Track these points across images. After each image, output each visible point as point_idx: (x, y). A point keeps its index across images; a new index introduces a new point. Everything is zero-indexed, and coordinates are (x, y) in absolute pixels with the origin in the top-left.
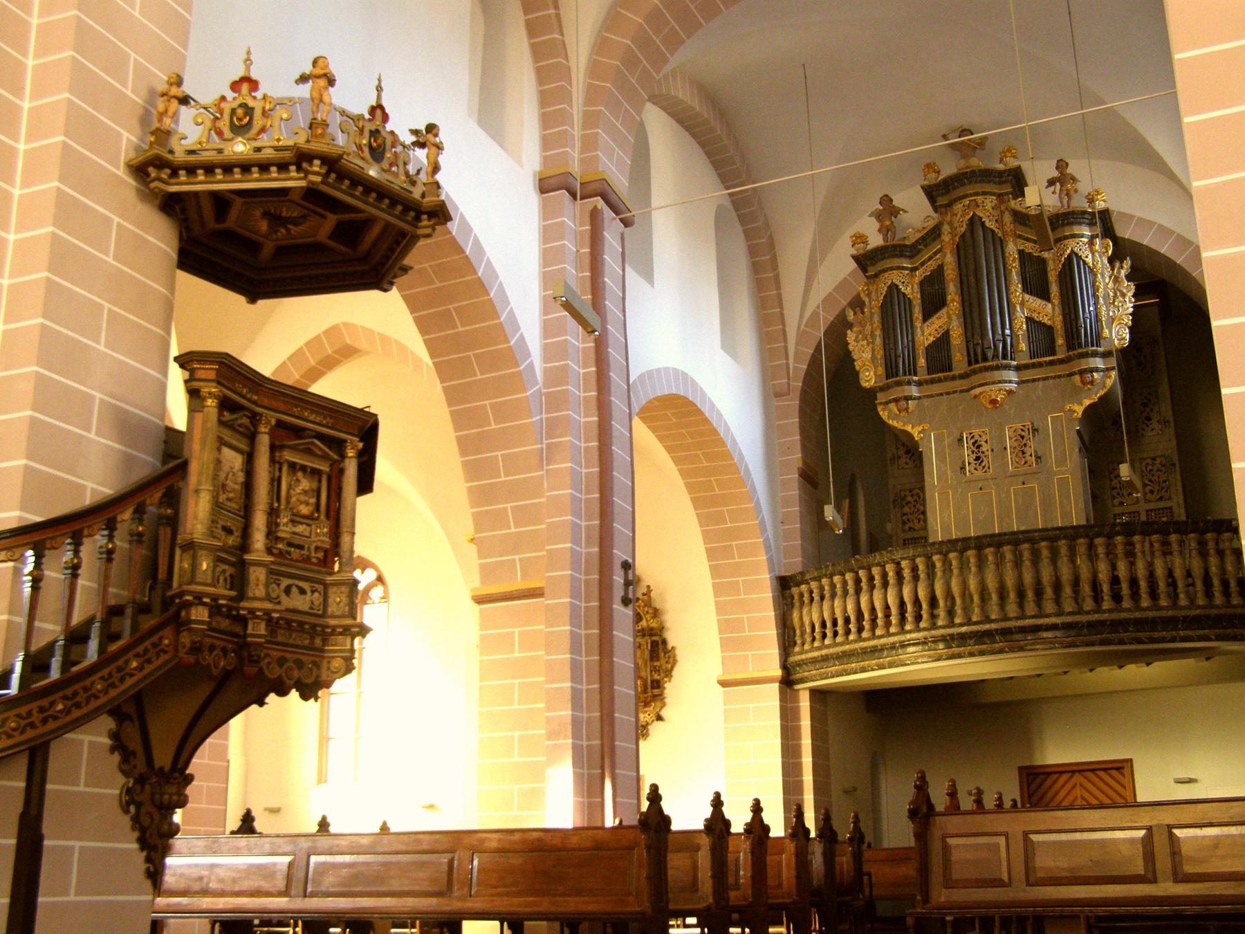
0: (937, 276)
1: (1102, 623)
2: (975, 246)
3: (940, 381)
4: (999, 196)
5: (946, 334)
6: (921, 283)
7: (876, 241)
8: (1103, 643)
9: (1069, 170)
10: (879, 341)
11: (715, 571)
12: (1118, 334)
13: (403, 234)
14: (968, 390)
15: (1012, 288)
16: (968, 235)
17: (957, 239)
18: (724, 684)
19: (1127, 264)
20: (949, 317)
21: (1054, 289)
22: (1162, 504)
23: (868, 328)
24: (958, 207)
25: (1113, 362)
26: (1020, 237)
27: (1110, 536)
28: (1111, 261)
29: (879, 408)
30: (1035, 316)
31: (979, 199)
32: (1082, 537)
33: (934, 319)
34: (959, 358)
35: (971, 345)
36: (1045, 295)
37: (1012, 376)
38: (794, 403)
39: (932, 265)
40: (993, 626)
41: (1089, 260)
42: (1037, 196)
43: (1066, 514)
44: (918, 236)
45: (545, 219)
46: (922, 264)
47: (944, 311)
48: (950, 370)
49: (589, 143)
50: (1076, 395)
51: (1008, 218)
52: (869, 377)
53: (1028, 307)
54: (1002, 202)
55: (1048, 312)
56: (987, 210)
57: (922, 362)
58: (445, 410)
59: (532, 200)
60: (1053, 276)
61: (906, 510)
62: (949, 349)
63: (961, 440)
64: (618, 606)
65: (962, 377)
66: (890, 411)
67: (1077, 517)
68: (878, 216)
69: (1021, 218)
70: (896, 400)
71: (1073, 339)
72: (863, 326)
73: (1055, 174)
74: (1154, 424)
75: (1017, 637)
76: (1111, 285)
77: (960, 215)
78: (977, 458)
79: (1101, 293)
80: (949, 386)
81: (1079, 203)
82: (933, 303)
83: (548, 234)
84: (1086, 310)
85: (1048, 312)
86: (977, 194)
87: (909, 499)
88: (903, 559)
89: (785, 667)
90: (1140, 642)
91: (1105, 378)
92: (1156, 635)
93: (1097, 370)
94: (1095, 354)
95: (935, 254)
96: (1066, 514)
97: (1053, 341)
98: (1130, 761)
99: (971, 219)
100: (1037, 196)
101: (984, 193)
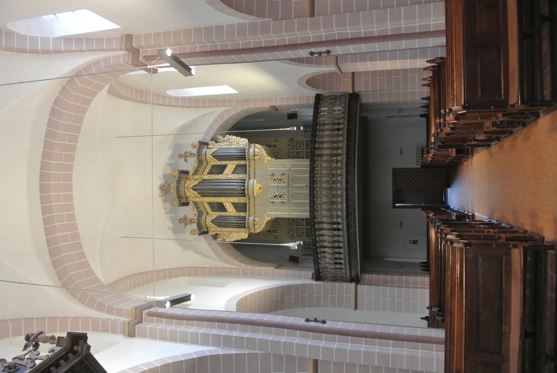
0: (211, 204)
1: (347, 153)
2: (203, 189)
3: (249, 208)
4: (187, 179)
5: (233, 204)
6: (213, 211)
7: (194, 226)
8: (354, 154)
9: (183, 153)
10: (231, 229)
11: (311, 306)
12: (243, 142)
13: (81, 362)
14: (255, 198)
15: (221, 178)
16: (199, 191)
17: (199, 196)
18: (356, 308)
19: (219, 137)
20: (227, 202)
21: (223, 163)
22: (305, 144)
23: (226, 233)
24: (188, 194)
25: (252, 145)
26: (203, 173)
27: (316, 230)
28: (217, 142)
29: (256, 232)
30: (232, 171)
31: (186, 186)
32: (314, 159)
33: (226, 208)
34: (242, 200)
35: (238, 195)
36: (225, 167)
37: (251, 181)
38: (250, 267)
39: (207, 206)
40: (344, 194)
41: (215, 150)
42: (190, 165)
43: (305, 166)
44: (195, 209)
45: (146, 337)
46: (206, 210)
47: (224, 204)
48: (246, 204)
49: (119, 312)
50: (261, 159)
51: (195, 177)
52: (243, 235)
53: (228, 174)
54: (189, 178)
55: (231, 165)
56: (191, 183)
57: (242, 214)
58: (75, 203)
59: (136, 341)
60: (219, 163)
61: (295, 235)
62: (239, 203)
63: (272, 202)
64: (326, 326)
65: (249, 200)
66: (258, 228)
67: (307, 162)
68: (186, 224)
69: (196, 172)
70: (254, 225)
71: (243, 158)
72: (225, 235)
73: (183, 158)
74: (276, 144)
75: (349, 186)
76: (225, 143)
77: (192, 195)
78: (280, 197)
79: (227, 147)
80: (252, 204)
81: (195, 151)
82: (221, 207)
83: (153, 336)
84: (235, 153)
85: (231, 165)
86: (184, 186)
87: (291, 233)
88: (314, 227)
89: (351, 281)
90: (355, 142)
91: (258, 149)
92: (353, 136)
93: (254, 150)
94: (249, 150)
95: (203, 205)
96: (305, 166)
97: (242, 165)
98: (393, 169)
99: (193, 190)
100: (190, 165)
101: (185, 184)
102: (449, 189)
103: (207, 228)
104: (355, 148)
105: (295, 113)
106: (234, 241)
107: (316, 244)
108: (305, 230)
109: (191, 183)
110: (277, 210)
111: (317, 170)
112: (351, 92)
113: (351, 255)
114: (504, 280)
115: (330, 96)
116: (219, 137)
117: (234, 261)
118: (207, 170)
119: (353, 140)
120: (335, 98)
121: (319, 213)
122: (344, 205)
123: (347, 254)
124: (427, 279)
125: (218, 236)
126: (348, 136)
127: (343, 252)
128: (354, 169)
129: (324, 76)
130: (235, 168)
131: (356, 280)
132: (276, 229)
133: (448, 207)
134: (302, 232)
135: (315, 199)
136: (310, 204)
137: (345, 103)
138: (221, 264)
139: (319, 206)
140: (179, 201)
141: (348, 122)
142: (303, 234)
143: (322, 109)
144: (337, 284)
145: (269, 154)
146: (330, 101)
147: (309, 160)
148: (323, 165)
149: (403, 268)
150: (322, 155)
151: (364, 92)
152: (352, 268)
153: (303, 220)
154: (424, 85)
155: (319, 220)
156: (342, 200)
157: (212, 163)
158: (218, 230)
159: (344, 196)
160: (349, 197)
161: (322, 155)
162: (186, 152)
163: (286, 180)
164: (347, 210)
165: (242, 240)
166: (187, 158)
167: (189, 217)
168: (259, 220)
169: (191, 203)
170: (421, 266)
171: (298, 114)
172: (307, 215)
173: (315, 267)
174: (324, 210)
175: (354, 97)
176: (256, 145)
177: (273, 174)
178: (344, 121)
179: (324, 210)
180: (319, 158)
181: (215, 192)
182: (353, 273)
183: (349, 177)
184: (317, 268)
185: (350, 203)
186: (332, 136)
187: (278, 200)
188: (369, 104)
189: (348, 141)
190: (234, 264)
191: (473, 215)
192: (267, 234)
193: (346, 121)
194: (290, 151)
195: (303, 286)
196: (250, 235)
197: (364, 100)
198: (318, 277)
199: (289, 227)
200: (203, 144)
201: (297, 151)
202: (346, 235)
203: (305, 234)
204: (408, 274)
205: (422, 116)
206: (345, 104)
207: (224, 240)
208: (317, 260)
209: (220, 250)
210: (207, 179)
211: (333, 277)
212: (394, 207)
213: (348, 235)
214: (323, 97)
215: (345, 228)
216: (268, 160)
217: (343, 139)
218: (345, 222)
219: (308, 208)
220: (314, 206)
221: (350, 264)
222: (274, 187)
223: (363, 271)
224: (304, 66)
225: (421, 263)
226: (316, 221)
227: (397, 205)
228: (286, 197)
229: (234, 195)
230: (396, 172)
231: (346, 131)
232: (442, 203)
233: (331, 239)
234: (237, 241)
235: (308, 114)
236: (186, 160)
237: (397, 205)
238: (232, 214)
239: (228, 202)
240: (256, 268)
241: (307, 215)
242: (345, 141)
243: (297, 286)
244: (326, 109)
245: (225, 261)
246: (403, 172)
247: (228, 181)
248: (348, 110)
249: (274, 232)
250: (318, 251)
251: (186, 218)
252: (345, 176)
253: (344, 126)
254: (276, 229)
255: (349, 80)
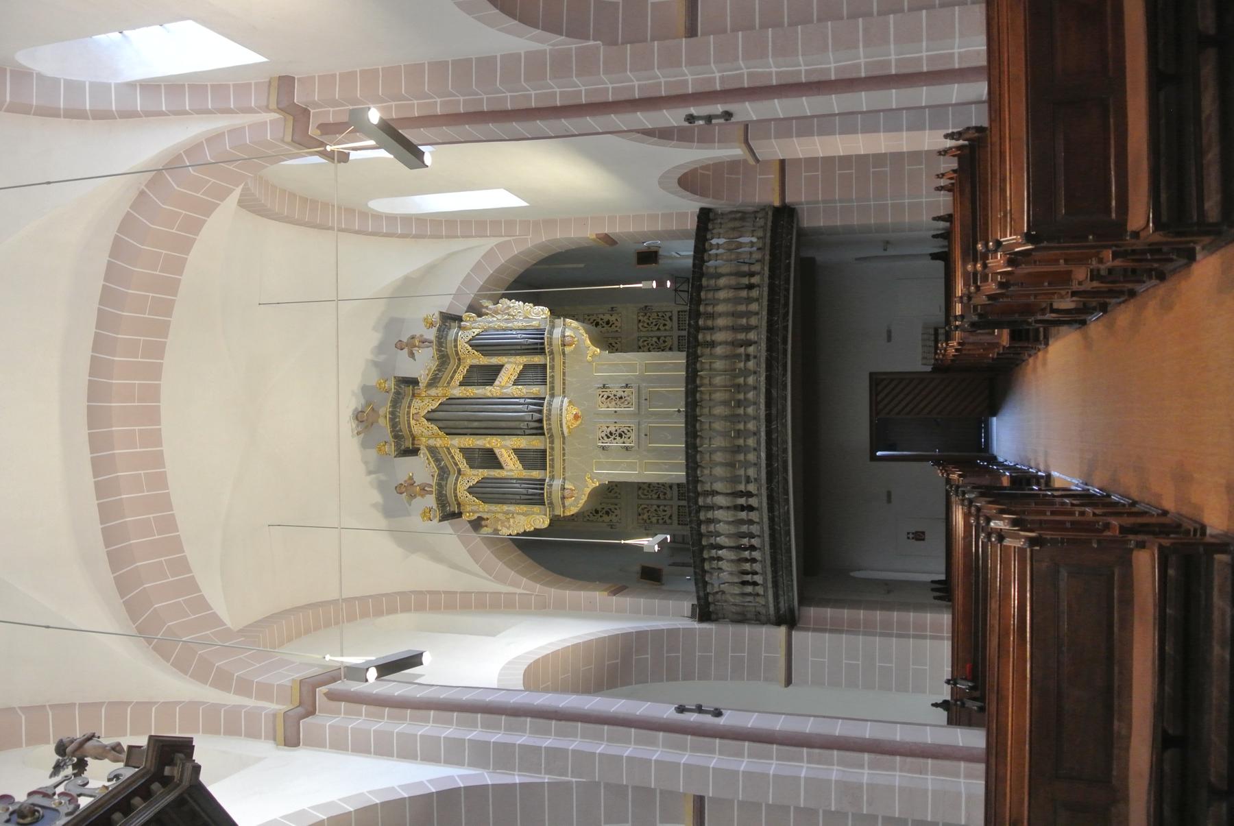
0: (467, 452)
1: (769, 340)
2: (450, 420)
3: (552, 460)
4: (413, 395)
5: (516, 451)
6: (471, 467)
7: (431, 501)
8: (785, 342)
9: (405, 340)
10: (512, 508)
11: (688, 677)
12: (539, 314)
14: (564, 437)
15: (489, 394)
16: (441, 424)
17: (441, 433)
18: (789, 682)
19: (486, 303)
20: (502, 447)
21: (494, 360)
22: (675, 318)
23: (500, 516)
24: (416, 430)
25: (559, 322)
26: (449, 383)
28: (480, 315)
29: (568, 513)
30: (513, 378)
31: (413, 411)
32: (696, 352)
33: (501, 460)
34: (535, 443)
35: (528, 432)
36: (498, 369)
37: (557, 401)
38: (553, 592)
39: (459, 457)
40: (763, 429)
41: (477, 331)
42: (421, 365)
43: (676, 367)
44: (433, 464)
45: (323, 746)
46: (456, 464)
47: (496, 451)
48: (544, 451)
49: (265, 692)
50: (579, 351)
51: (433, 392)
52: (539, 520)
53: (505, 384)
54: (419, 395)
55: (512, 366)
56: (423, 404)
57: (536, 474)
59: (301, 755)
60: (485, 361)
61: (654, 520)
62: (529, 450)
63: (603, 448)
64: (721, 721)
65: (552, 442)
66: (571, 505)
67: (680, 359)
68: (412, 496)
69: (434, 382)
70: (563, 498)
71: (538, 349)
72: (498, 520)
73: (406, 350)
74: (612, 319)
75: (774, 411)
76: (499, 317)
77: (426, 433)
78: (621, 436)
79: (504, 325)
80: (557, 452)
81: (431, 334)
82: (489, 459)
83: (339, 744)
84: (520, 338)
85: (512, 366)
86: (408, 413)
87: (645, 517)
88: (696, 503)
89: (778, 623)
90: (787, 313)
91: (572, 330)
92: (782, 301)
93: (563, 332)
94: (551, 333)
95: (450, 453)
96: (676, 367)
97: (535, 366)
98: (871, 374)
99: (428, 420)
100: (421, 365)
101: (409, 407)
102: (994, 419)
103: (459, 504)
104: (786, 328)
105: (653, 249)
106: (518, 534)
107: (700, 541)
108: (675, 509)
109: (423, 404)
110: (614, 466)
111: (702, 377)
112: (777, 203)
113: (777, 564)
114: (1116, 620)
115: (731, 212)
116: (486, 303)
117: (519, 577)
118: (459, 377)
119: (782, 311)
120: (742, 217)
121: (707, 472)
122: (763, 455)
123: (768, 562)
124: (946, 618)
125: (483, 523)
126: (771, 301)
127: (759, 558)
128: (785, 374)
129: (718, 168)
130: (521, 372)
131: (789, 620)
132: (612, 507)
133: (993, 459)
134: (668, 513)
135: (698, 440)
136: (687, 453)
137: (764, 227)
138: (491, 586)
139: (707, 456)
140: (397, 445)
141: (772, 270)
142: (670, 517)
143: (714, 241)
144: (746, 630)
145: (596, 341)
146: (731, 225)
147: (684, 354)
148: (716, 365)
149: (892, 594)
150: (712, 344)
151: (807, 203)
152: (781, 592)
153: (671, 487)
154: (939, 189)
155: (707, 487)
156: (758, 442)
157: (469, 362)
158: (483, 509)
159: (763, 434)
160: (774, 436)
161: (712, 344)
162: (413, 337)
163: (634, 399)
164: (769, 465)
165: (537, 532)
166: (415, 350)
167: (419, 480)
168: (574, 488)
169: (423, 450)
170: (933, 590)
171: (661, 252)
172: (679, 475)
173: (698, 592)
174: (717, 464)
175: (784, 215)
176: (568, 320)
177: (604, 386)
178: (763, 269)
179: (717, 464)
180: (707, 351)
181: (476, 424)
182: (782, 604)
183: (774, 392)
184: (702, 594)
185: (775, 449)
186: (737, 301)
187: (617, 443)
188: (817, 231)
189: (771, 312)
190: (518, 586)
191: (1049, 476)
192: (592, 518)
193: (766, 269)
194: (642, 334)
195: (672, 633)
196: (555, 520)
197: (806, 222)
198: (704, 613)
199: (641, 502)
200: (449, 319)
201: (658, 334)
202: (766, 519)
203: (675, 518)
204: (905, 606)
205: (935, 256)
206: (765, 231)
207: (496, 531)
208: (703, 576)
209: (487, 553)
210: (458, 395)
211: (737, 613)
212: (874, 458)
213: (771, 519)
214: (716, 214)
215: (765, 505)
216: (594, 355)
217: (759, 308)
218: (764, 492)
219: (682, 460)
220: (695, 456)
221: (775, 584)
222: (607, 414)
223: (803, 601)
224: (674, 146)
225: (933, 582)
226: (699, 489)
227: (879, 453)
228: (633, 435)
229: (519, 432)
230: (878, 381)
231: (766, 289)
232: (980, 450)
233: (732, 530)
234: (525, 533)
235: (682, 252)
236: (412, 355)
237: (879, 453)
238: (515, 474)
239: (506, 447)
240: (568, 593)
241: (679, 475)
242: (765, 313)
243: (657, 633)
244: (721, 241)
245: (500, 579)
246: (892, 380)
247: (505, 401)
248: (772, 244)
249: (607, 513)
250: (706, 555)
251: (411, 482)
252: (763, 390)
253: (762, 279)
254: (612, 507)
255: (774, 176)
